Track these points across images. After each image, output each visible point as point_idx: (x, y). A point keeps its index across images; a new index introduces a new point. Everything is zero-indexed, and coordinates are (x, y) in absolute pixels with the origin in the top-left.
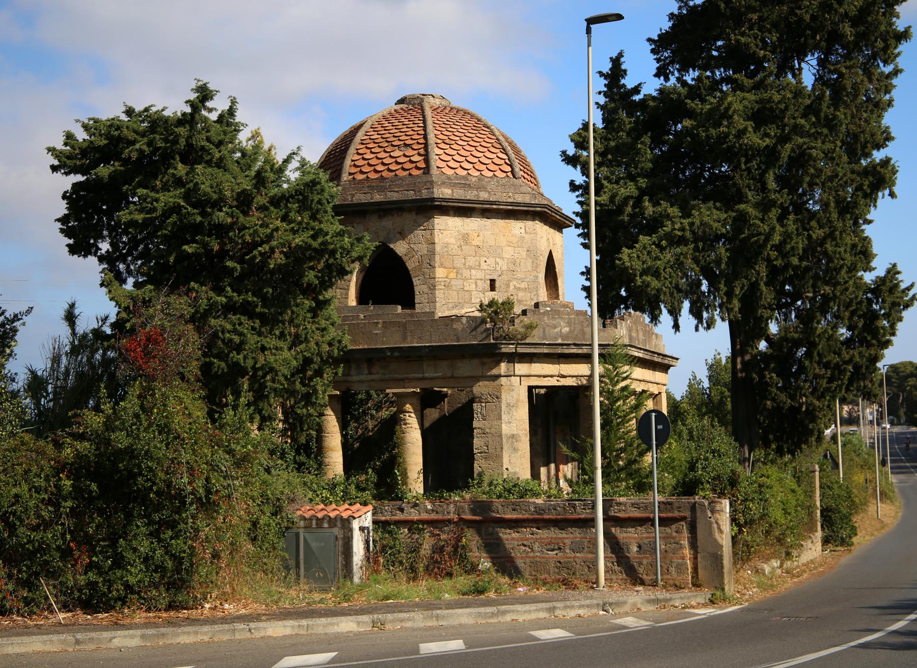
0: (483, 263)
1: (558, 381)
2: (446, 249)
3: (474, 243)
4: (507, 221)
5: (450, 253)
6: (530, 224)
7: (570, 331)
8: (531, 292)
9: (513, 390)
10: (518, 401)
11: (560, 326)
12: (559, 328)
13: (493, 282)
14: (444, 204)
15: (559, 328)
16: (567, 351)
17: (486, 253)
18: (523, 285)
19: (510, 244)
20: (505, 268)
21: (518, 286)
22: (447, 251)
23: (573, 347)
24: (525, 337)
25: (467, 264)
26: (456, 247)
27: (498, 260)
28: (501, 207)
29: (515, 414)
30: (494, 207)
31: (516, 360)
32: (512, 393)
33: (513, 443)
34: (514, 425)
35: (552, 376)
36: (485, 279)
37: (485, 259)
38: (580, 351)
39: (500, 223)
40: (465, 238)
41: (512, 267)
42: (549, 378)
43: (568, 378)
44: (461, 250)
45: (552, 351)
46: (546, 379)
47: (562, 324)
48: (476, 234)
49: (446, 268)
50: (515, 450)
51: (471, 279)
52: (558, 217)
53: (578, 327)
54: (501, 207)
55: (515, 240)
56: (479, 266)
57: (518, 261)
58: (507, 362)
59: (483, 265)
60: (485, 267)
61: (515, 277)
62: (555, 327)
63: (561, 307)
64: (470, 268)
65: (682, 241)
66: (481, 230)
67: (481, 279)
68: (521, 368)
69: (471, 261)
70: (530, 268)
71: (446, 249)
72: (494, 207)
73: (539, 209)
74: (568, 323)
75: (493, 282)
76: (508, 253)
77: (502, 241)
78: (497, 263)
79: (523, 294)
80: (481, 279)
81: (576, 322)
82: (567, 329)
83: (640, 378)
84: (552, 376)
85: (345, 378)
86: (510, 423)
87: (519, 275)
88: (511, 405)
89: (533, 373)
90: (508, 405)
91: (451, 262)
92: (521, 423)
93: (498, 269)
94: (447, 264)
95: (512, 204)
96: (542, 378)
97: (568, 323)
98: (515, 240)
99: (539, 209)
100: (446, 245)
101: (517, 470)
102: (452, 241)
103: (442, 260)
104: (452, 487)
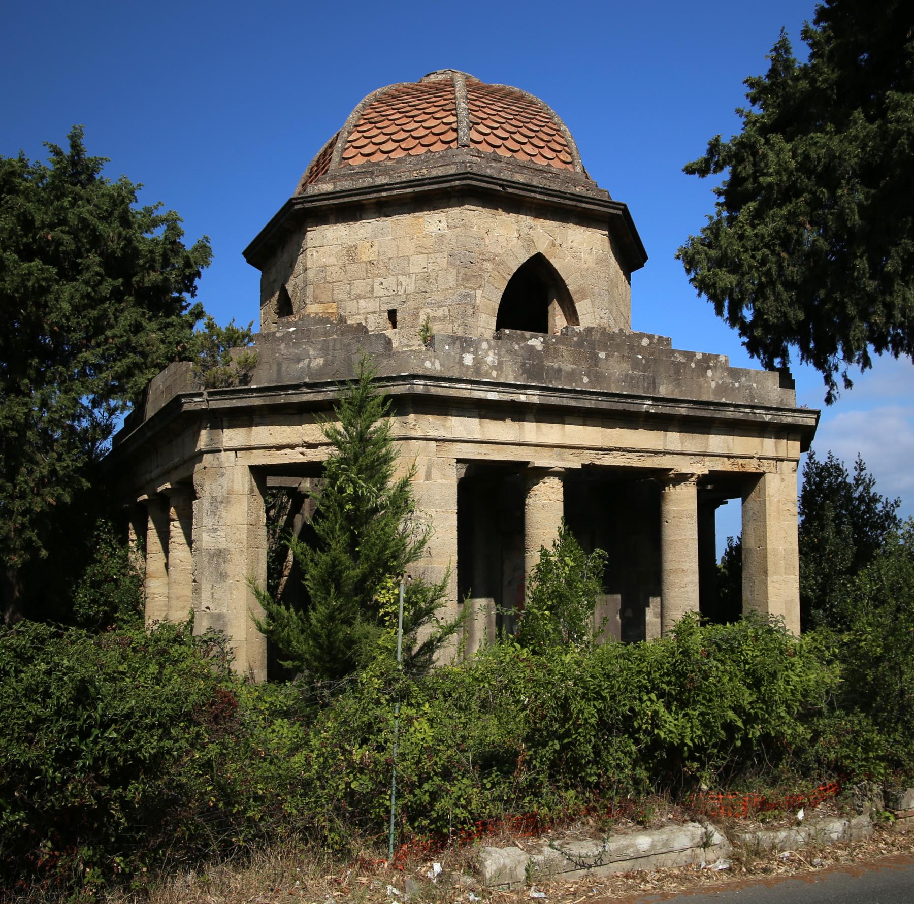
0: (377, 287)
1: (302, 453)
2: (323, 275)
3: (365, 258)
4: (417, 214)
5: (328, 279)
6: (455, 212)
7: (326, 364)
8: (453, 322)
9: (223, 475)
10: (230, 492)
11: (308, 356)
12: (306, 361)
13: (392, 314)
14: (307, 205)
15: (306, 361)
16: (296, 399)
17: (383, 271)
18: (440, 313)
19: (421, 250)
20: (411, 288)
21: (432, 314)
22: (325, 278)
23: (305, 390)
24: (245, 380)
25: (353, 293)
26: (337, 269)
27: (401, 278)
28: (395, 192)
29: (224, 514)
30: (384, 194)
31: (226, 423)
32: (221, 480)
33: (218, 564)
34: (222, 534)
35: (292, 447)
36: (381, 312)
37: (381, 279)
38: (320, 397)
39: (404, 222)
40: (351, 253)
41: (423, 285)
42: (288, 451)
43: (320, 448)
44: (345, 272)
45: (268, 401)
46: (282, 452)
47: (311, 352)
48: (369, 245)
49: (322, 303)
50: (223, 576)
51: (358, 314)
52: (538, 196)
53: (341, 354)
54: (395, 192)
55: (428, 242)
56: (372, 291)
57: (433, 275)
58: (211, 428)
59: (378, 289)
60: (381, 293)
61: (429, 300)
62: (299, 360)
63: (316, 323)
64: (358, 297)
65: (789, 193)
66: (376, 237)
67: (374, 313)
68: (232, 437)
69: (360, 287)
70: (452, 283)
71: (323, 275)
72: (384, 194)
73: (457, 183)
74: (322, 349)
75: (392, 314)
76: (418, 264)
77: (408, 247)
78: (399, 284)
79: (441, 326)
80: (374, 313)
81: (338, 346)
82: (321, 361)
83: (679, 448)
84: (292, 447)
85: (178, 475)
86: (215, 530)
87: (435, 297)
88: (219, 499)
89: (254, 443)
90: (214, 499)
91: (329, 294)
92: (235, 530)
93: (401, 292)
94: (324, 297)
95: (410, 183)
96: (273, 451)
97: (322, 349)
98: (428, 242)
99: (457, 183)
100: (323, 268)
101: (225, 611)
102: (333, 260)
103: (317, 292)
104: (721, 619)
